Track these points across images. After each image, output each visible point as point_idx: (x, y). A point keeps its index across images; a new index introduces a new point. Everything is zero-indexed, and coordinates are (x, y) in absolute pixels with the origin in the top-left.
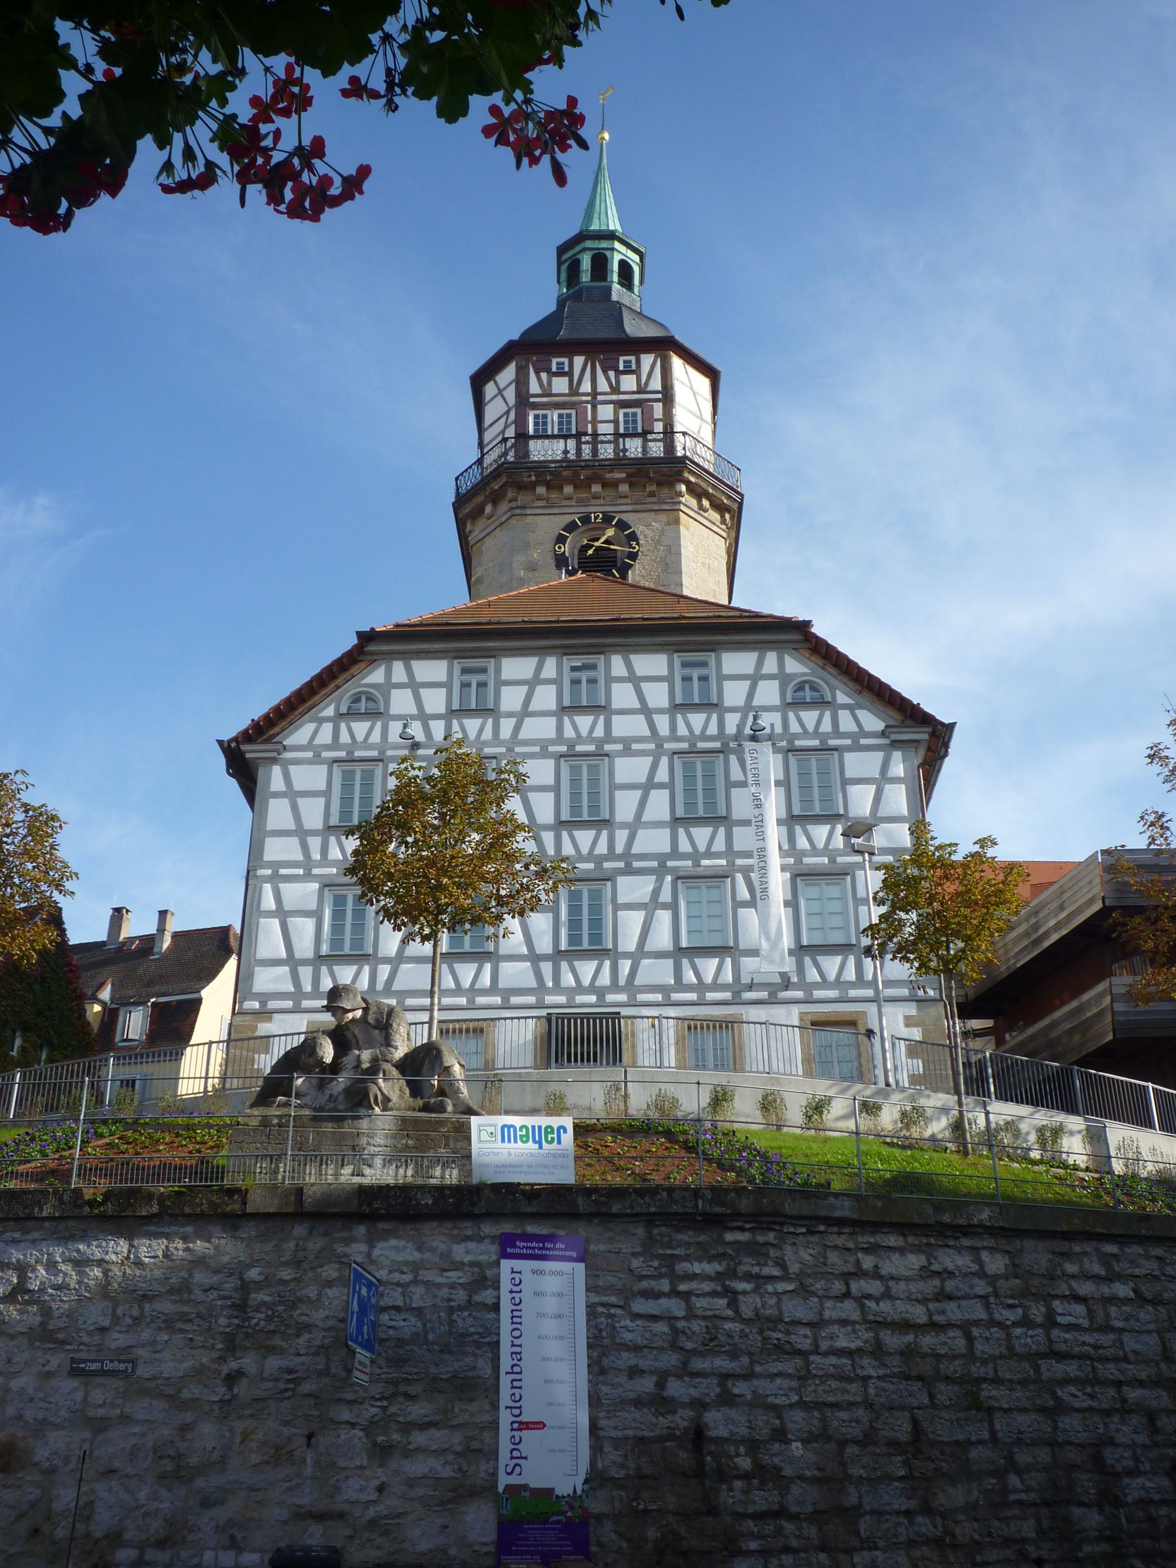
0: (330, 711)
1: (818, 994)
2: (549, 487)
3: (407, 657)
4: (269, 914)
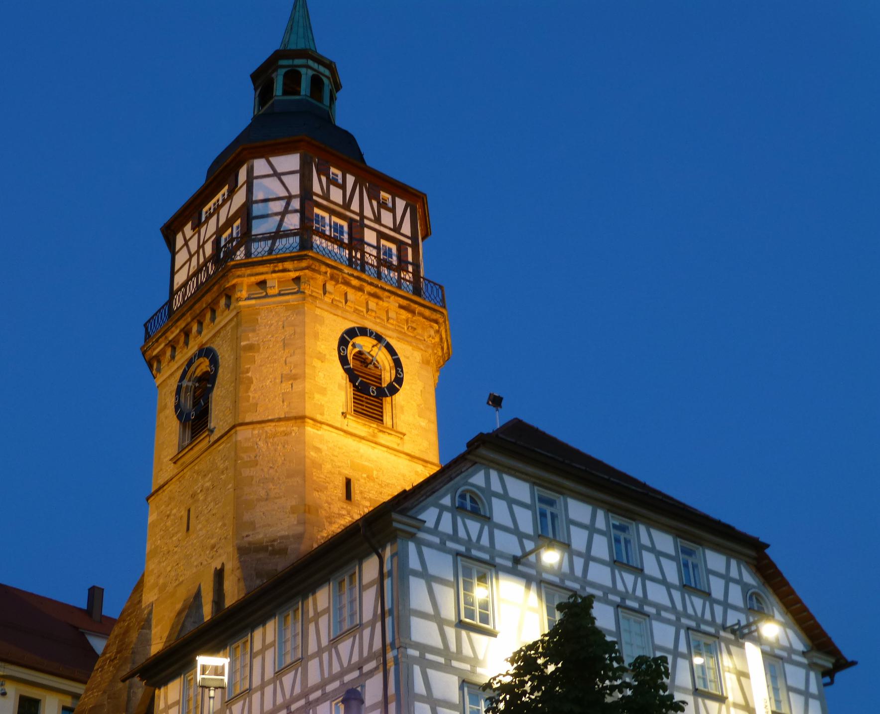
0: (447, 501)
4: (422, 699)
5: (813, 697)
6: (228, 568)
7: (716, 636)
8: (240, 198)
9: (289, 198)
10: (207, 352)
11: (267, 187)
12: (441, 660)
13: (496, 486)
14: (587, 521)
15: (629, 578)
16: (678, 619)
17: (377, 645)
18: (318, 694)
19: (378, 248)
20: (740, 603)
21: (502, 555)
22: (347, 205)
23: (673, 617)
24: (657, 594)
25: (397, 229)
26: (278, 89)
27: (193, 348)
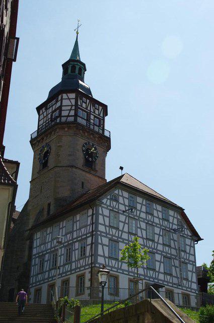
0: (109, 197)
1: (130, 274)
2: (83, 131)
3: (122, 190)
5: (194, 272)
6: (52, 203)
7: (169, 231)
8: (59, 104)
9: (72, 106)
10: (48, 145)
11: (65, 102)
12: (105, 235)
13: (120, 194)
14: (141, 202)
15: (150, 216)
16: (161, 227)
17: (91, 230)
18: (76, 240)
19: (94, 120)
20: (176, 223)
21: (121, 210)
22: (87, 108)
23: (159, 226)
24: (156, 220)
25: (99, 115)
26: (69, 71)
27: (44, 144)
